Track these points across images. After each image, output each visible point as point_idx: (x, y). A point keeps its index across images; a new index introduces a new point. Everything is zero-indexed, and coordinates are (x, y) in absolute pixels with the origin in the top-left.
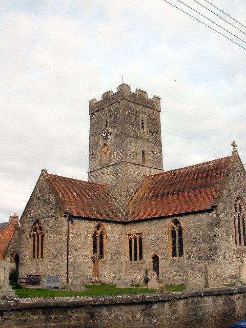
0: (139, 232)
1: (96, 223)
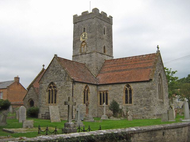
0: (106, 90)
1: (85, 85)
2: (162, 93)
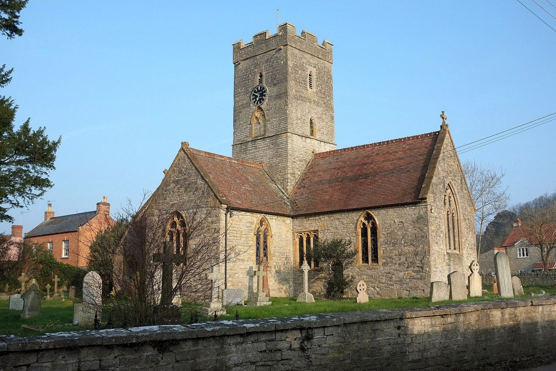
2: (456, 234)
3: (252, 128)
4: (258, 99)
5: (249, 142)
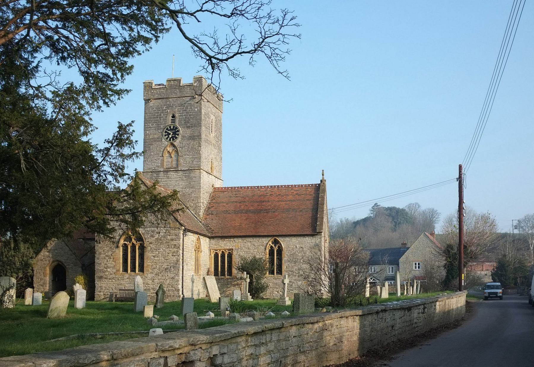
3: (163, 160)
4: (170, 136)
5: (161, 171)
